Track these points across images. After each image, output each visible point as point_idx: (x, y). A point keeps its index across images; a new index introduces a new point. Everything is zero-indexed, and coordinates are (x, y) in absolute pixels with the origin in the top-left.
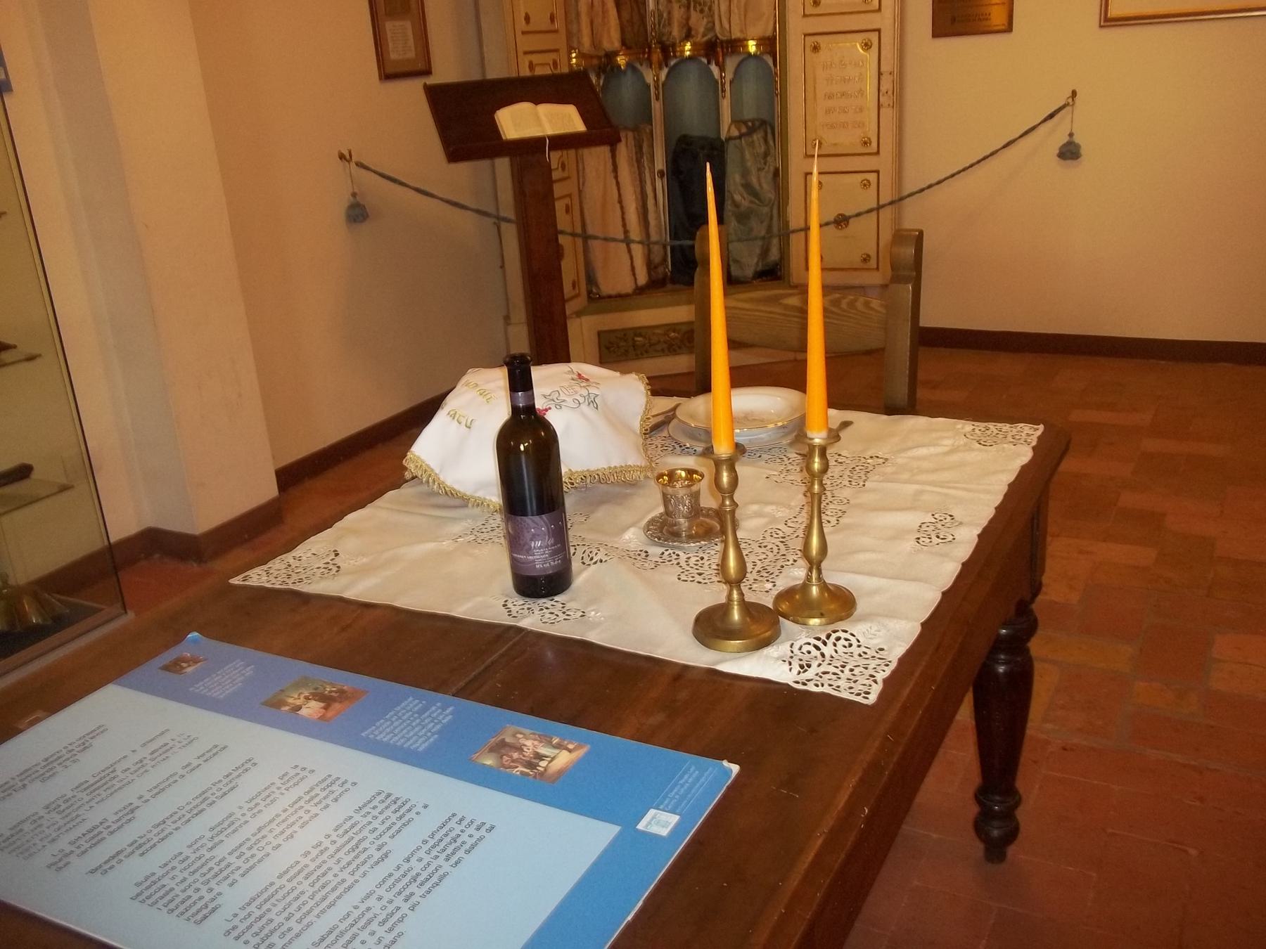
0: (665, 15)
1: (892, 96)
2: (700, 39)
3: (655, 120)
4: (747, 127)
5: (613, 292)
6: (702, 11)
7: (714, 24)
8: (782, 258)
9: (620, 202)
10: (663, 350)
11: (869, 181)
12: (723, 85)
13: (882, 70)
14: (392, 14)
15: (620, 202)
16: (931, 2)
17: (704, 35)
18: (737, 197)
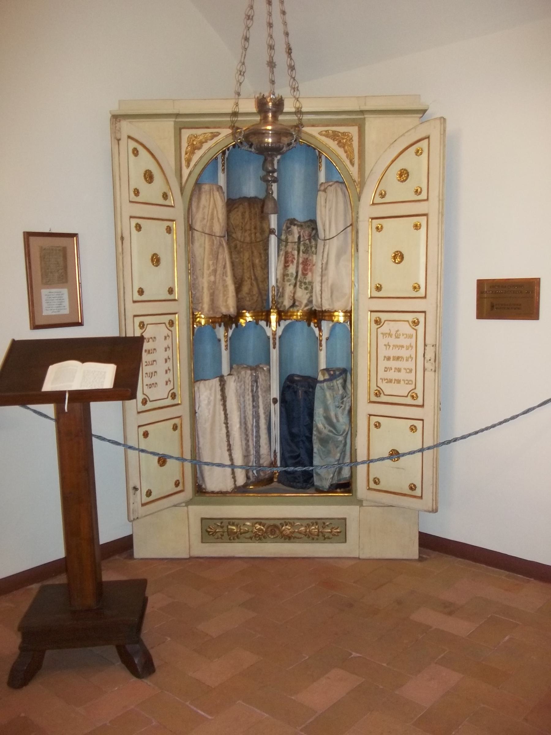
0: (281, 290)
1: (434, 363)
3: (272, 359)
4: (330, 375)
5: (217, 490)
6: (306, 289)
8: (351, 476)
9: (226, 423)
10: (251, 538)
11: (415, 427)
12: (321, 341)
13: (427, 343)
14: (48, 283)
15: (226, 423)
18: (320, 426)
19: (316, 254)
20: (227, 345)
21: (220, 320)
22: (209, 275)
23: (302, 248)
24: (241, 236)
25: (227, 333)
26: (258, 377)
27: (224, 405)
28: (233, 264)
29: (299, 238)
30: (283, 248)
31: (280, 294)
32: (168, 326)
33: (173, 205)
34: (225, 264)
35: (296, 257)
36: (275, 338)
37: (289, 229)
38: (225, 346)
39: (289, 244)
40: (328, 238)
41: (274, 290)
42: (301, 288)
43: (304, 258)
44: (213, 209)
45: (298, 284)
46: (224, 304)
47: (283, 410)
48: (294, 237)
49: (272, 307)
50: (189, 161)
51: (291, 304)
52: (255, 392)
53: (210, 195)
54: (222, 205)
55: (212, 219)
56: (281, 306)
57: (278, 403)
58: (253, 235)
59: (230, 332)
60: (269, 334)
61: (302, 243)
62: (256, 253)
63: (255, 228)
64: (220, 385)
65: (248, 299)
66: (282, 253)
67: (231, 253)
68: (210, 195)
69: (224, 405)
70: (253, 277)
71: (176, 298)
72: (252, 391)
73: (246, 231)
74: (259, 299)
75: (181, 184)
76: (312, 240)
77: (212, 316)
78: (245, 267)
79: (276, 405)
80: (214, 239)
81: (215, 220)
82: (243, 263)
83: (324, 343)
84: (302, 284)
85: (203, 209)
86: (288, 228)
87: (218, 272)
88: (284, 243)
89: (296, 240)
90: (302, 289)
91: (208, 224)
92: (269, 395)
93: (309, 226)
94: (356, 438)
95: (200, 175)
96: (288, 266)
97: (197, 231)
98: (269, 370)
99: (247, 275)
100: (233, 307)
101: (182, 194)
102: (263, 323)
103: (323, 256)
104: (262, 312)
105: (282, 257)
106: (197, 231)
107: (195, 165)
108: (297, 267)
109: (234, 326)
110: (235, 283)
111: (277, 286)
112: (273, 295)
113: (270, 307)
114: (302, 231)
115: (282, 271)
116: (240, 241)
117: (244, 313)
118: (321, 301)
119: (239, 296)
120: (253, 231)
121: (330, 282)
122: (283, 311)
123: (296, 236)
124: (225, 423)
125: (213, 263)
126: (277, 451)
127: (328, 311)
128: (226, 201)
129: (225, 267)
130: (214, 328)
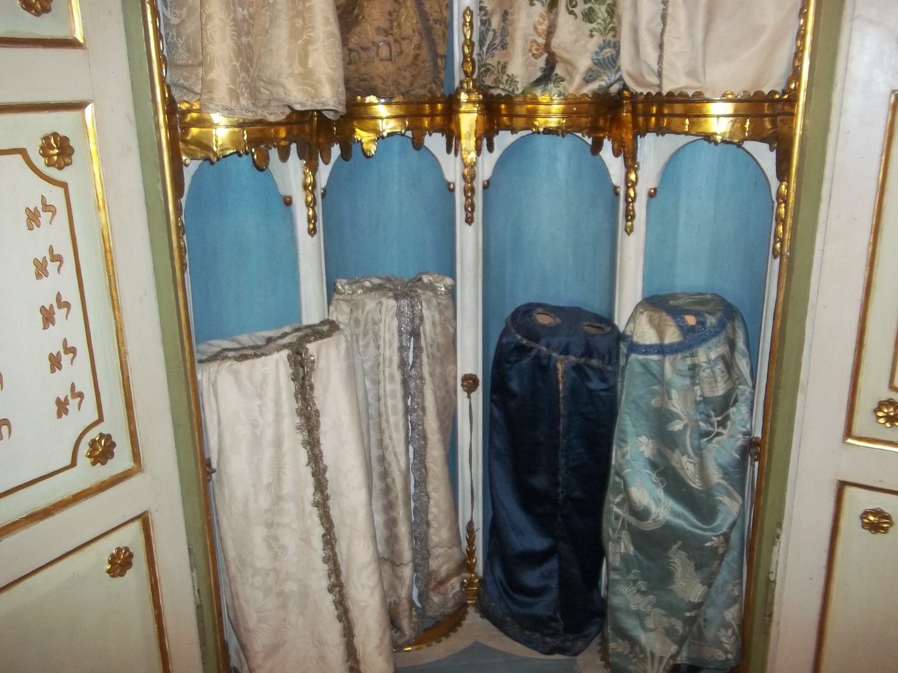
0: (495, 22)
2: (575, 86)
6: (589, 16)
7: (618, 53)
12: (630, 201)
20: (315, 217)
21: (283, 133)
25: (314, 175)
26: (422, 319)
27: (313, 444)
31: (494, 38)
32: (40, 162)
36: (472, 190)
38: (309, 221)
41: (471, 23)
42: (571, 13)
46: (298, 69)
47: (497, 413)
49: (461, 82)
52: (412, 366)
56: (497, 81)
57: (480, 388)
59: (324, 172)
60: (452, 170)
64: (295, 378)
69: (313, 444)
71: (79, 36)
72: (403, 364)
74: (425, 54)
77: (250, 116)
79: (473, 395)
83: (640, 208)
92: (451, 367)
94: (775, 548)
98: (452, 292)
100: (332, 81)
102: (435, 142)
104: (433, 102)
109: (336, 150)
111: (481, 9)
112: (465, 43)
117: (371, 104)
119: (354, 41)
122: (509, 99)
124: (316, 504)
126: (476, 527)
127: (681, 94)
130: (261, 166)
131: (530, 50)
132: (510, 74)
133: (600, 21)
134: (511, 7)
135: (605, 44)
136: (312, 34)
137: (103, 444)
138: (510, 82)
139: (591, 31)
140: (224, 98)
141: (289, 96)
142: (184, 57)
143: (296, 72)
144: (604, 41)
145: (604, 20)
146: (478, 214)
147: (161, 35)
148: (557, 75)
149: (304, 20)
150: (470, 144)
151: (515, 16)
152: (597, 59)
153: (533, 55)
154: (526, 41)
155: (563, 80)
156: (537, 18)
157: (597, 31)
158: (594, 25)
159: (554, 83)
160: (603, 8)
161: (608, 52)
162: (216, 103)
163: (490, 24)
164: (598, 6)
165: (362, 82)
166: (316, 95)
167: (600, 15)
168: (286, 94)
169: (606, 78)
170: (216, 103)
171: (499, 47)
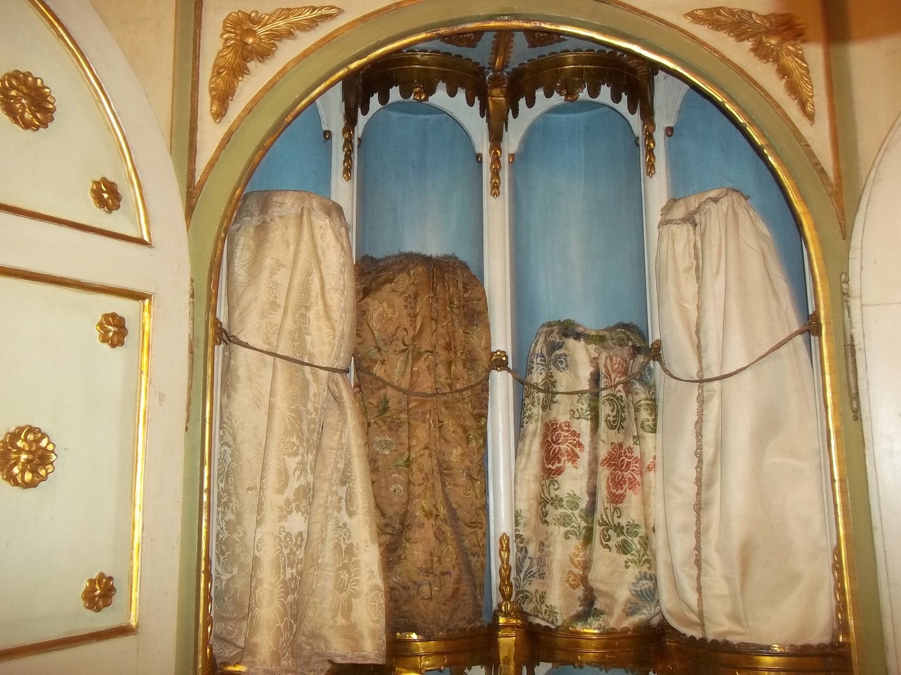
0: (532, 549)
6: (624, 548)
16: (175, 2)
17: (630, 611)
19: (654, 430)
22: (285, 512)
23: (605, 410)
24: (403, 374)
28: (373, 464)
29: (595, 378)
30: (537, 410)
31: (531, 566)
33: (146, 239)
34: (348, 464)
35: (585, 440)
37: (558, 352)
39: (558, 397)
40: (717, 374)
42: (607, 547)
43: (612, 444)
44: (309, 274)
45: (598, 529)
46: (341, 621)
48: (577, 376)
49: (500, 605)
50: (223, 98)
51: (578, 608)
53: (300, 225)
54: (342, 260)
55: (304, 305)
58: (442, 370)
61: (604, 393)
62: (450, 425)
63: (448, 347)
65: (425, 589)
66: (534, 427)
67: (367, 427)
68: (300, 225)
70: (443, 511)
71: (134, 624)
73: (418, 356)
74: (465, 588)
75: (191, 172)
76: (638, 386)
78: (418, 477)
80: (310, 377)
81: (315, 313)
82: (408, 463)
84: (611, 532)
85: (273, 273)
86: (553, 347)
87: (320, 500)
88: (541, 395)
89: (585, 385)
90: (609, 548)
91: (289, 325)
93: (621, 343)
95: (264, 149)
96: (559, 471)
97: (246, 345)
99: (422, 503)
101: (190, 210)
103: (699, 434)
105: (531, 442)
106: (246, 345)
107: (249, 111)
108: (593, 473)
110: (381, 530)
111: (518, 536)
113: (495, 606)
114: (604, 355)
115: (534, 487)
116: (398, 389)
118: (700, 600)
120: (443, 355)
121: (737, 532)
123: (585, 372)
125: (302, 464)
128: (354, 263)
129: (345, 479)
131: (568, 581)
132: (549, 605)
133: (634, 552)
134: (547, 539)
135: (641, 576)
136: (356, 588)
137: (105, 190)
138: (548, 613)
139: (626, 562)
140: (265, 662)
141: (330, 649)
142: (230, 609)
143: (339, 624)
144: (640, 572)
145: (638, 551)
146: (505, 187)
147: (211, 597)
148: (596, 609)
149: (349, 573)
150: (509, 668)
151: (551, 549)
152: (635, 591)
153: (571, 585)
154: (563, 572)
155: (603, 613)
156: (572, 550)
157: (631, 562)
158: (629, 556)
159: (594, 617)
160: (636, 540)
161: (646, 584)
162: (256, 667)
163: (526, 551)
164: (630, 538)
165: (402, 619)
166: (357, 648)
167: (634, 547)
168: (326, 647)
169: (645, 611)
170: (256, 667)
171: (536, 575)
